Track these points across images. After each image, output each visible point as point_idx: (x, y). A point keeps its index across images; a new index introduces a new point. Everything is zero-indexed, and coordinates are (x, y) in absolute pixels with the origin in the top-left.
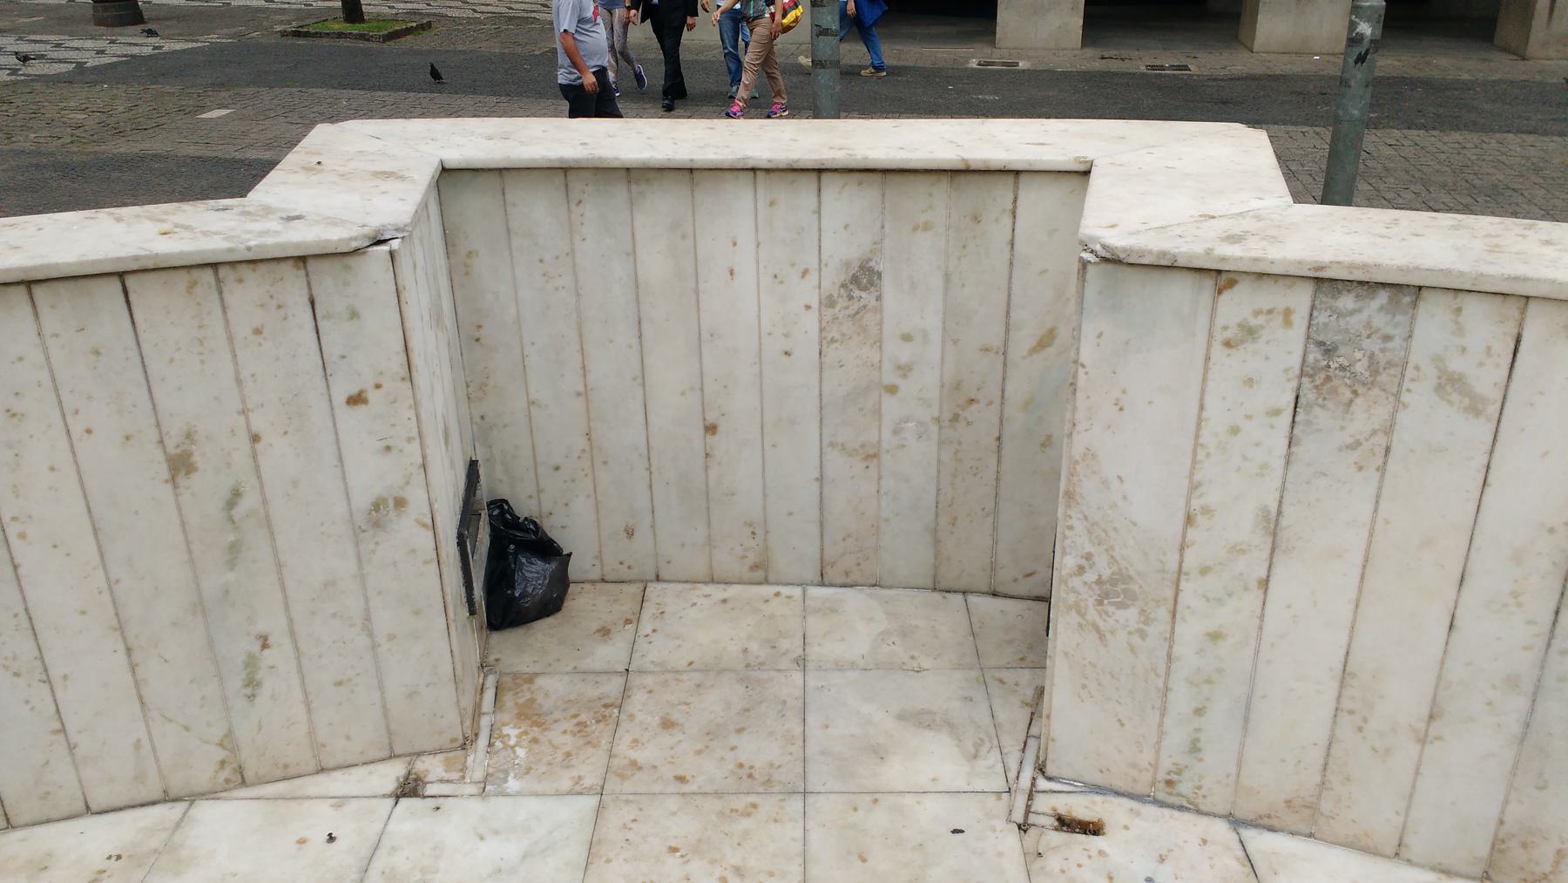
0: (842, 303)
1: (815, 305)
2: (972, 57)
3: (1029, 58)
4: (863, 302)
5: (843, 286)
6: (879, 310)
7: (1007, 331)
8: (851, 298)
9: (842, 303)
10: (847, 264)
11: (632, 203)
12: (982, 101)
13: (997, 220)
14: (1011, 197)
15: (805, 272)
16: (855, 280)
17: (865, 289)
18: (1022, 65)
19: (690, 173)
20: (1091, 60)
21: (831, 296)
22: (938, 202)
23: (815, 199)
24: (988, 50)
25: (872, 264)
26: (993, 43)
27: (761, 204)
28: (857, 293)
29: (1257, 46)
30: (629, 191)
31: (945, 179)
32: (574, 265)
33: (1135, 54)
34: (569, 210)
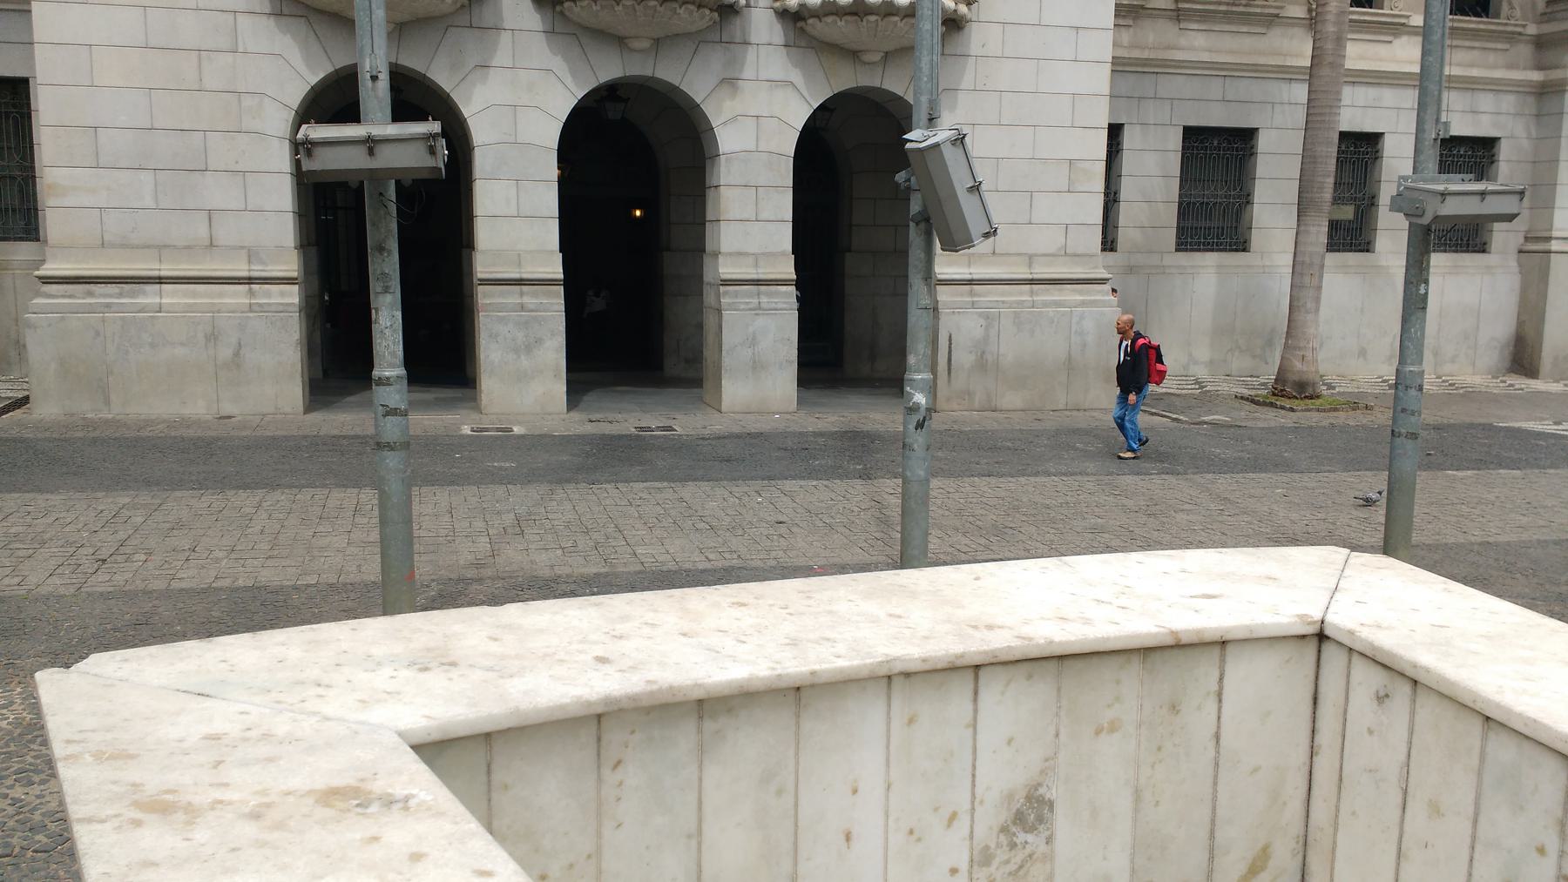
0: (1001, 855)
1: (964, 866)
2: (463, 423)
3: (519, 423)
4: (1028, 850)
5: (1004, 830)
6: (1049, 858)
7: (1211, 858)
8: (1013, 846)
9: (1001, 855)
10: (1010, 797)
11: (701, 750)
12: (501, 468)
13: (1199, 708)
14: (1217, 674)
15: (953, 817)
16: (1019, 818)
17: (1031, 829)
18: (517, 430)
19: (796, 697)
20: (579, 424)
21: (987, 847)
22: (1127, 693)
23: (970, 707)
24: (475, 416)
25: (1041, 791)
26: (478, 409)
27: (896, 724)
28: (1021, 837)
29: (725, 405)
30: (700, 731)
31: (1136, 661)
32: (600, 872)
33: (619, 417)
34: (600, 780)
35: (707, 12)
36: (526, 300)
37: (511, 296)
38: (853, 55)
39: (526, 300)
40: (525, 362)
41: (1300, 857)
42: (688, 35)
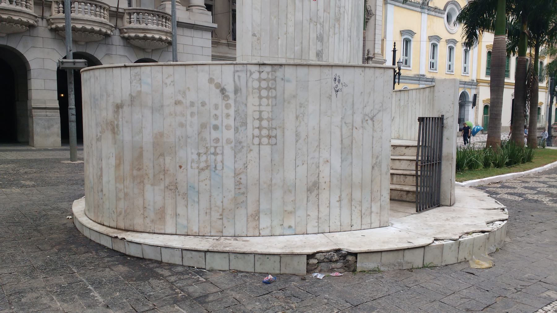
35: (24, 26)
36: (48, 113)
37: (43, 113)
38: (143, 50)
39: (48, 113)
40: (48, 132)
41: (238, 255)
42: (95, 42)
